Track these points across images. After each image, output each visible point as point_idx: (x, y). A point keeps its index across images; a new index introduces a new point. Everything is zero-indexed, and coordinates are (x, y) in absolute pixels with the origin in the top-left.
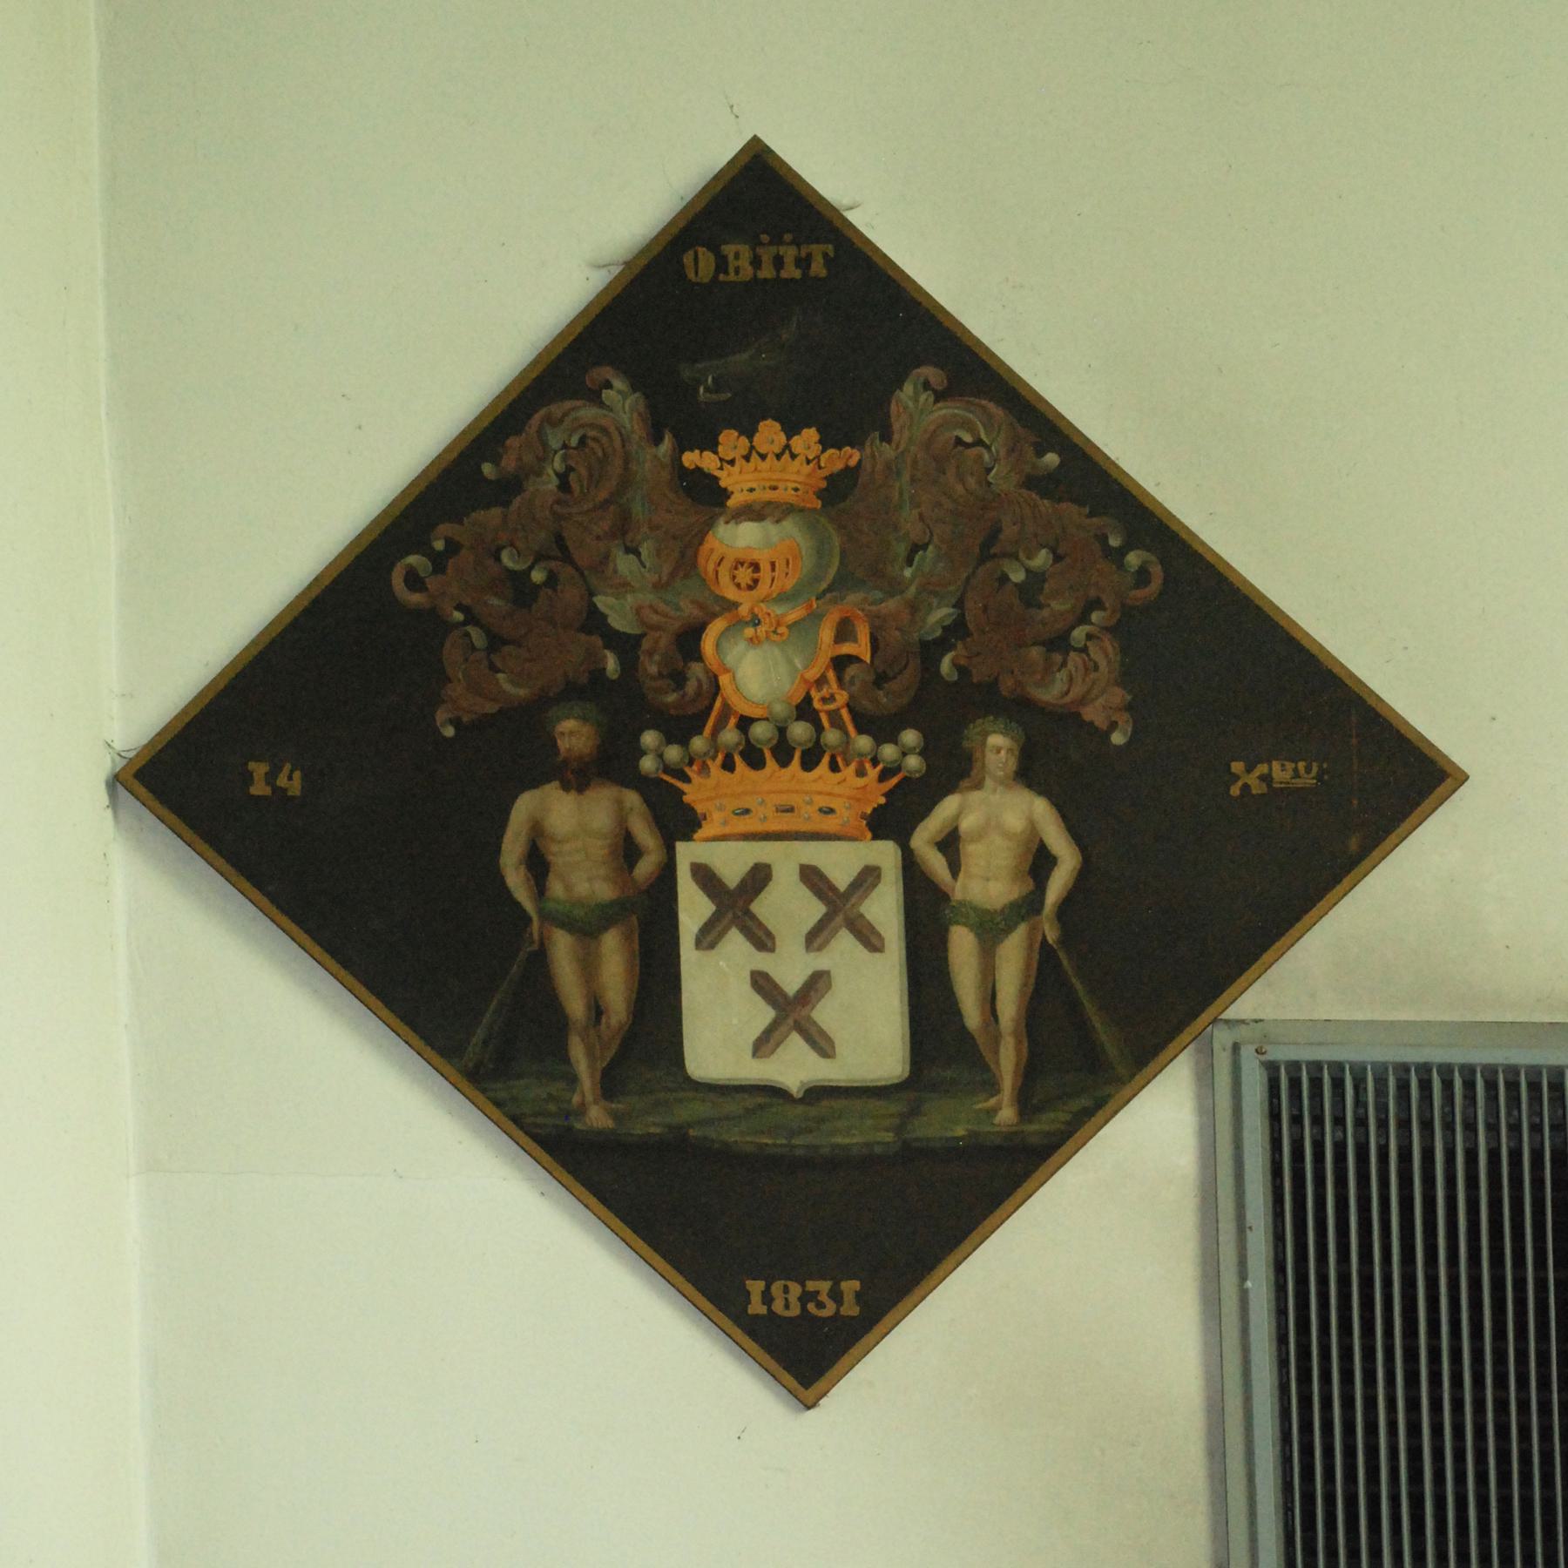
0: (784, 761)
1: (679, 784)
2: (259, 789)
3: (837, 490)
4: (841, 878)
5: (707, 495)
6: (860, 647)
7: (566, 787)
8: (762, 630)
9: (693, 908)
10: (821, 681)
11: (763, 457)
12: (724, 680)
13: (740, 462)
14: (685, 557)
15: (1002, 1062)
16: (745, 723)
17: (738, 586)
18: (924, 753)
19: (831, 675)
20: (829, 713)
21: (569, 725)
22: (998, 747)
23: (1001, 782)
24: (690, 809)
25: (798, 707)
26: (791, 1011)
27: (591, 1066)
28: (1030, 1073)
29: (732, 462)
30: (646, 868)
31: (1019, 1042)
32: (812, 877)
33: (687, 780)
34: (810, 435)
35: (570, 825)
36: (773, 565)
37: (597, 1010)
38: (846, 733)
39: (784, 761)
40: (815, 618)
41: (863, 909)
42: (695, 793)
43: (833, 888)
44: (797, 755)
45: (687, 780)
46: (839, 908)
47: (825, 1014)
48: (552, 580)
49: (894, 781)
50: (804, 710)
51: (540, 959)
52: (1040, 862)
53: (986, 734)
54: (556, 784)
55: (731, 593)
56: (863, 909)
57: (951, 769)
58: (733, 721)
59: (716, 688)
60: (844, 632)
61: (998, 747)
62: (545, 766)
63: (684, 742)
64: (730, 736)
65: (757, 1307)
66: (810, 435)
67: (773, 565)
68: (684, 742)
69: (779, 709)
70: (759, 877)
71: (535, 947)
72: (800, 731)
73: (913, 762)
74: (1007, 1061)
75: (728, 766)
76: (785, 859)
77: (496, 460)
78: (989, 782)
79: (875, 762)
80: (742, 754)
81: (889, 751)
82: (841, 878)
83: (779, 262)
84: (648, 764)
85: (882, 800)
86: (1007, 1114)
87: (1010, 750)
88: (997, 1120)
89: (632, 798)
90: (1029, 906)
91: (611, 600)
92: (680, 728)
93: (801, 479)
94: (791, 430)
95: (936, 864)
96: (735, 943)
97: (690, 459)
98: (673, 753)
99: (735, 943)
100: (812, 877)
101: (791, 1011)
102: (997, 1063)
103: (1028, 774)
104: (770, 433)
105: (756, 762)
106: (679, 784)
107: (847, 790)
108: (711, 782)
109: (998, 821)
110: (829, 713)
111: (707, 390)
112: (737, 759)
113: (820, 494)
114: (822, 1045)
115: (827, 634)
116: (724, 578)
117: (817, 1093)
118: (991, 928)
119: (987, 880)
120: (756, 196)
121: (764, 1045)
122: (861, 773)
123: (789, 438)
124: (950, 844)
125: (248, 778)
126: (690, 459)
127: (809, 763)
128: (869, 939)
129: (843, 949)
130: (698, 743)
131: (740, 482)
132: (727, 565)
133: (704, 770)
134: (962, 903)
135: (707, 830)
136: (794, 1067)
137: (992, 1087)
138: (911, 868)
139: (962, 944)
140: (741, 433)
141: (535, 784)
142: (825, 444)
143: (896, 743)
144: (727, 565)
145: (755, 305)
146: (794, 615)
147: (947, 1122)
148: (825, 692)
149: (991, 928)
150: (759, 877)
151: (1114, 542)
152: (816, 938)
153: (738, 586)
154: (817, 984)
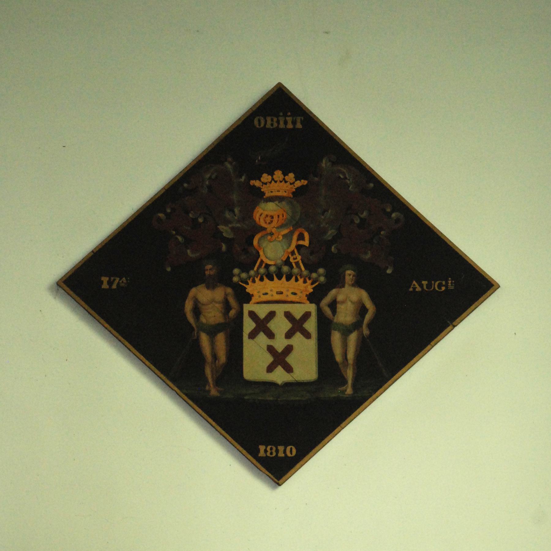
0: (280, 278)
1: (244, 285)
2: (105, 286)
3: (298, 193)
4: (262, 316)
5: (258, 196)
6: (306, 243)
7: (208, 288)
8: (274, 237)
9: (249, 325)
10: (293, 253)
11: (276, 182)
12: (261, 253)
13: (288, 184)
14: (248, 214)
15: (348, 375)
16: (267, 266)
17: (266, 222)
18: (326, 276)
19: (296, 251)
20: (295, 263)
21: (209, 267)
22: (349, 274)
23: (349, 285)
24: (249, 293)
25: (285, 261)
26: (280, 359)
27: (212, 377)
28: (356, 379)
29: (266, 184)
30: (232, 313)
31: (354, 369)
32: (288, 315)
33: (248, 284)
34: (291, 176)
35: (208, 300)
36: (278, 216)
37: (215, 357)
38: (301, 269)
39: (280, 278)
40: (291, 233)
41: (268, 325)
42: (250, 288)
43: (259, 319)
44: (284, 276)
45: (248, 284)
46: (297, 326)
47: (269, 359)
48: (205, 220)
49: (317, 284)
50: (287, 262)
51: (197, 342)
52: (362, 310)
53: (344, 271)
54: (204, 285)
55: (263, 224)
56: (268, 325)
57: (335, 281)
58: (264, 265)
59: (259, 256)
60: (301, 237)
61: (349, 274)
62: (198, 279)
63: (248, 272)
64: (262, 270)
65: (262, 454)
66: (291, 176)
67: (278, 216)
68: (248, 272)
69: (279, 262)
70: (272, 315)
71: (195, 338)
72: (285, 269)
73: (322, 279)
74: (349, 374)
75: (262, 279)
76: (280, 309)
77: (188, 183)
78: (346, 286)
79: (310, 279)
80: (276, 275)
81: (314, 275)
82: (262, 316)
83: (286, 123)
84: (235, 279)
85: (312, 290)
86: (349, 391)
87: (353, 276)
88: (346, 393)
89: (229, 290)
90: (357, 325)
91: (223, 227)
92: (246, 267)
93: (287, 188)
94: (285, 174)
95: (328, 311)
96: (262, 338)
97: (252, 182)
98: (244, 275)
99: (262, 338)
100: (288, 315)
101: (280, 359)
102: (346, 374)
103: (358, 283)
104: (278, 174)
105: (271, 279)
106: (244, 285)
107: (304, 287)
108: (256, 285)
109: (350, 299)
110: (295, 263)
111: (258, 161)
112: (265, 277)
113: (293, 193)
114: (289, 369)
115: (295, 237)
116: (262, 220)
117: (287, 385)
118: (346, 331)
119: (345, 315)
120: (279, 100)
121: (270, 369)
122: (305, 282)
123: (272, 176)
124: (333, 305)
125: (102, 282)
126: (252, 182)
127: (288, 279)
128: (307, 335)
129: (298, 339)
130: (252, 273)
131: (269, 190)
132: (263, 216)
133: (254, 281)
134: (336, 323)
135: (254, 300)
136: (279, 376)
137: (344, 382)
138: (320, 312)
139: (336, 338)
140: (269, 174)
141: (196, 285)
142: (297, 178)
143: (234, 276)
144: (263, 216)
145: (279, 137)
146: (285, 231)
147: (329, 393)
148: (295, 256)
149: (346, 331)
150: (272, 315)
151: (388, 210)
152: (289, 335)
153: (266, 222)
154: (289, 349)
